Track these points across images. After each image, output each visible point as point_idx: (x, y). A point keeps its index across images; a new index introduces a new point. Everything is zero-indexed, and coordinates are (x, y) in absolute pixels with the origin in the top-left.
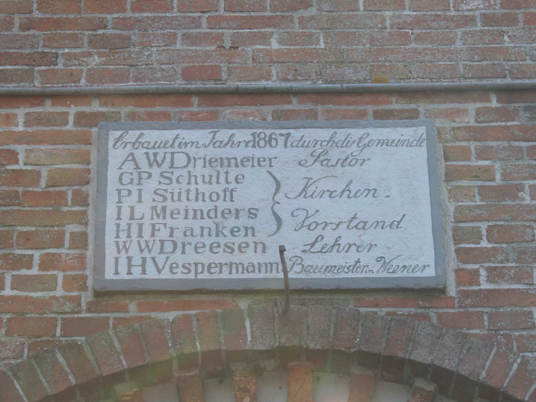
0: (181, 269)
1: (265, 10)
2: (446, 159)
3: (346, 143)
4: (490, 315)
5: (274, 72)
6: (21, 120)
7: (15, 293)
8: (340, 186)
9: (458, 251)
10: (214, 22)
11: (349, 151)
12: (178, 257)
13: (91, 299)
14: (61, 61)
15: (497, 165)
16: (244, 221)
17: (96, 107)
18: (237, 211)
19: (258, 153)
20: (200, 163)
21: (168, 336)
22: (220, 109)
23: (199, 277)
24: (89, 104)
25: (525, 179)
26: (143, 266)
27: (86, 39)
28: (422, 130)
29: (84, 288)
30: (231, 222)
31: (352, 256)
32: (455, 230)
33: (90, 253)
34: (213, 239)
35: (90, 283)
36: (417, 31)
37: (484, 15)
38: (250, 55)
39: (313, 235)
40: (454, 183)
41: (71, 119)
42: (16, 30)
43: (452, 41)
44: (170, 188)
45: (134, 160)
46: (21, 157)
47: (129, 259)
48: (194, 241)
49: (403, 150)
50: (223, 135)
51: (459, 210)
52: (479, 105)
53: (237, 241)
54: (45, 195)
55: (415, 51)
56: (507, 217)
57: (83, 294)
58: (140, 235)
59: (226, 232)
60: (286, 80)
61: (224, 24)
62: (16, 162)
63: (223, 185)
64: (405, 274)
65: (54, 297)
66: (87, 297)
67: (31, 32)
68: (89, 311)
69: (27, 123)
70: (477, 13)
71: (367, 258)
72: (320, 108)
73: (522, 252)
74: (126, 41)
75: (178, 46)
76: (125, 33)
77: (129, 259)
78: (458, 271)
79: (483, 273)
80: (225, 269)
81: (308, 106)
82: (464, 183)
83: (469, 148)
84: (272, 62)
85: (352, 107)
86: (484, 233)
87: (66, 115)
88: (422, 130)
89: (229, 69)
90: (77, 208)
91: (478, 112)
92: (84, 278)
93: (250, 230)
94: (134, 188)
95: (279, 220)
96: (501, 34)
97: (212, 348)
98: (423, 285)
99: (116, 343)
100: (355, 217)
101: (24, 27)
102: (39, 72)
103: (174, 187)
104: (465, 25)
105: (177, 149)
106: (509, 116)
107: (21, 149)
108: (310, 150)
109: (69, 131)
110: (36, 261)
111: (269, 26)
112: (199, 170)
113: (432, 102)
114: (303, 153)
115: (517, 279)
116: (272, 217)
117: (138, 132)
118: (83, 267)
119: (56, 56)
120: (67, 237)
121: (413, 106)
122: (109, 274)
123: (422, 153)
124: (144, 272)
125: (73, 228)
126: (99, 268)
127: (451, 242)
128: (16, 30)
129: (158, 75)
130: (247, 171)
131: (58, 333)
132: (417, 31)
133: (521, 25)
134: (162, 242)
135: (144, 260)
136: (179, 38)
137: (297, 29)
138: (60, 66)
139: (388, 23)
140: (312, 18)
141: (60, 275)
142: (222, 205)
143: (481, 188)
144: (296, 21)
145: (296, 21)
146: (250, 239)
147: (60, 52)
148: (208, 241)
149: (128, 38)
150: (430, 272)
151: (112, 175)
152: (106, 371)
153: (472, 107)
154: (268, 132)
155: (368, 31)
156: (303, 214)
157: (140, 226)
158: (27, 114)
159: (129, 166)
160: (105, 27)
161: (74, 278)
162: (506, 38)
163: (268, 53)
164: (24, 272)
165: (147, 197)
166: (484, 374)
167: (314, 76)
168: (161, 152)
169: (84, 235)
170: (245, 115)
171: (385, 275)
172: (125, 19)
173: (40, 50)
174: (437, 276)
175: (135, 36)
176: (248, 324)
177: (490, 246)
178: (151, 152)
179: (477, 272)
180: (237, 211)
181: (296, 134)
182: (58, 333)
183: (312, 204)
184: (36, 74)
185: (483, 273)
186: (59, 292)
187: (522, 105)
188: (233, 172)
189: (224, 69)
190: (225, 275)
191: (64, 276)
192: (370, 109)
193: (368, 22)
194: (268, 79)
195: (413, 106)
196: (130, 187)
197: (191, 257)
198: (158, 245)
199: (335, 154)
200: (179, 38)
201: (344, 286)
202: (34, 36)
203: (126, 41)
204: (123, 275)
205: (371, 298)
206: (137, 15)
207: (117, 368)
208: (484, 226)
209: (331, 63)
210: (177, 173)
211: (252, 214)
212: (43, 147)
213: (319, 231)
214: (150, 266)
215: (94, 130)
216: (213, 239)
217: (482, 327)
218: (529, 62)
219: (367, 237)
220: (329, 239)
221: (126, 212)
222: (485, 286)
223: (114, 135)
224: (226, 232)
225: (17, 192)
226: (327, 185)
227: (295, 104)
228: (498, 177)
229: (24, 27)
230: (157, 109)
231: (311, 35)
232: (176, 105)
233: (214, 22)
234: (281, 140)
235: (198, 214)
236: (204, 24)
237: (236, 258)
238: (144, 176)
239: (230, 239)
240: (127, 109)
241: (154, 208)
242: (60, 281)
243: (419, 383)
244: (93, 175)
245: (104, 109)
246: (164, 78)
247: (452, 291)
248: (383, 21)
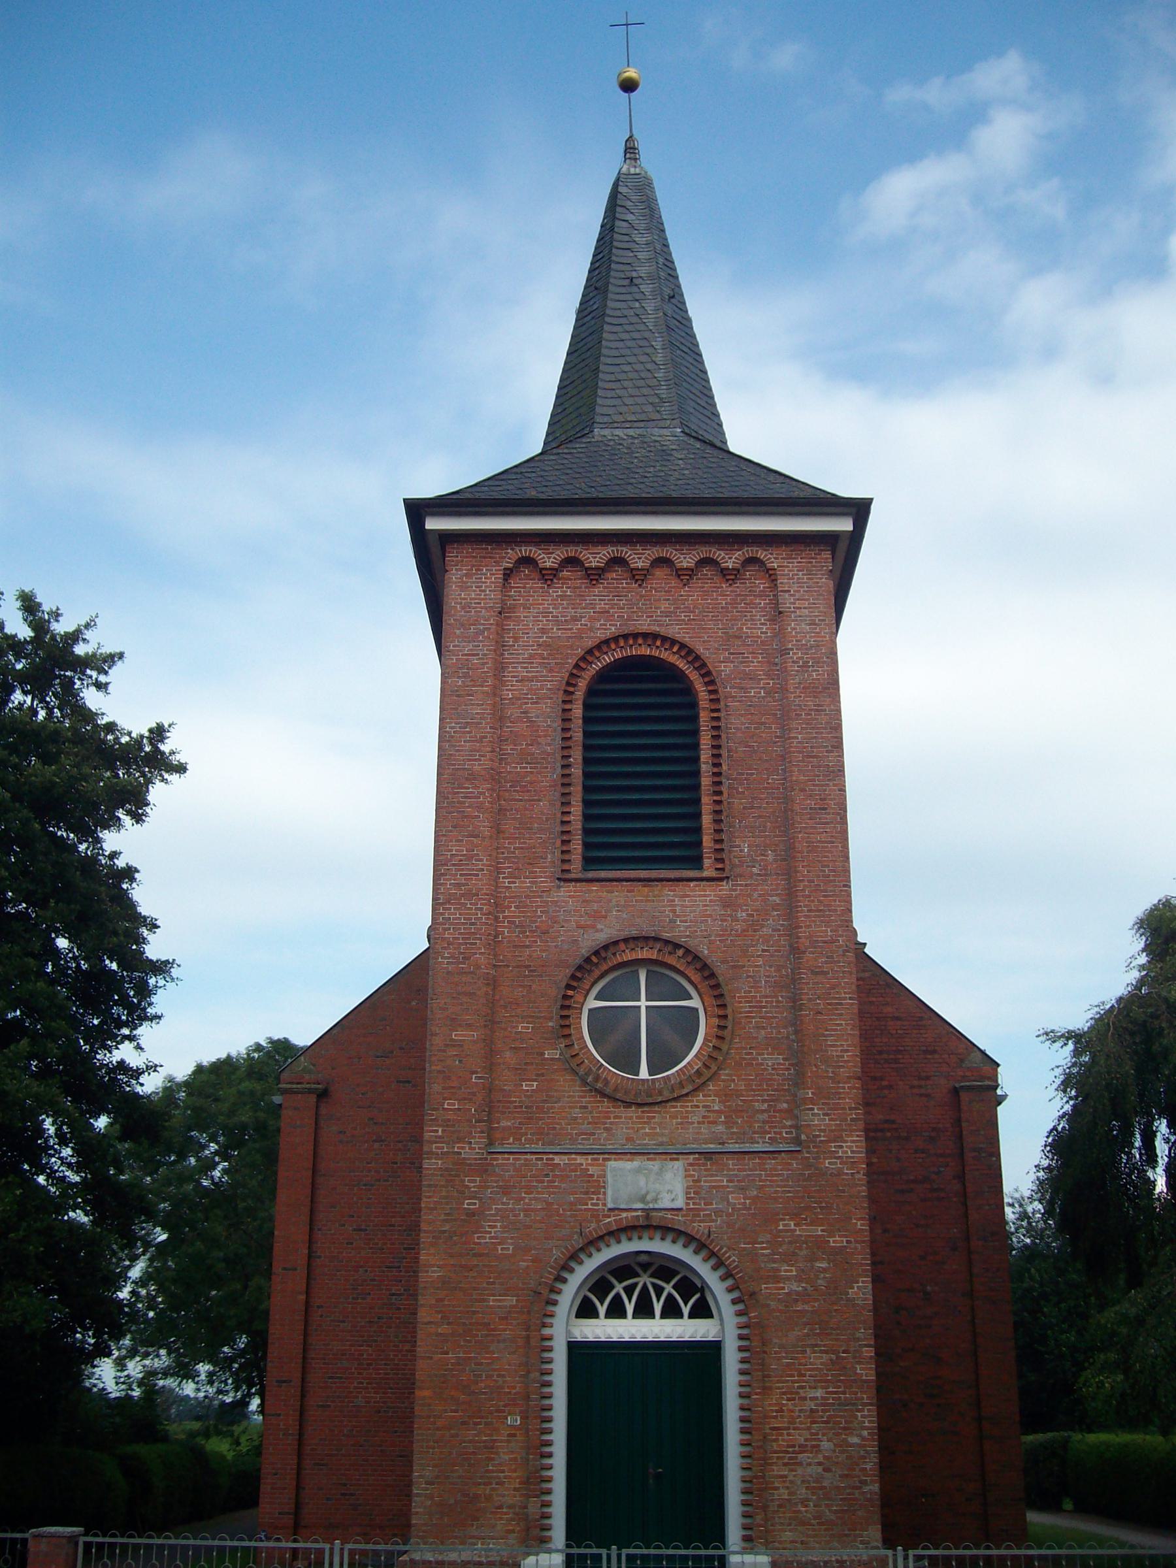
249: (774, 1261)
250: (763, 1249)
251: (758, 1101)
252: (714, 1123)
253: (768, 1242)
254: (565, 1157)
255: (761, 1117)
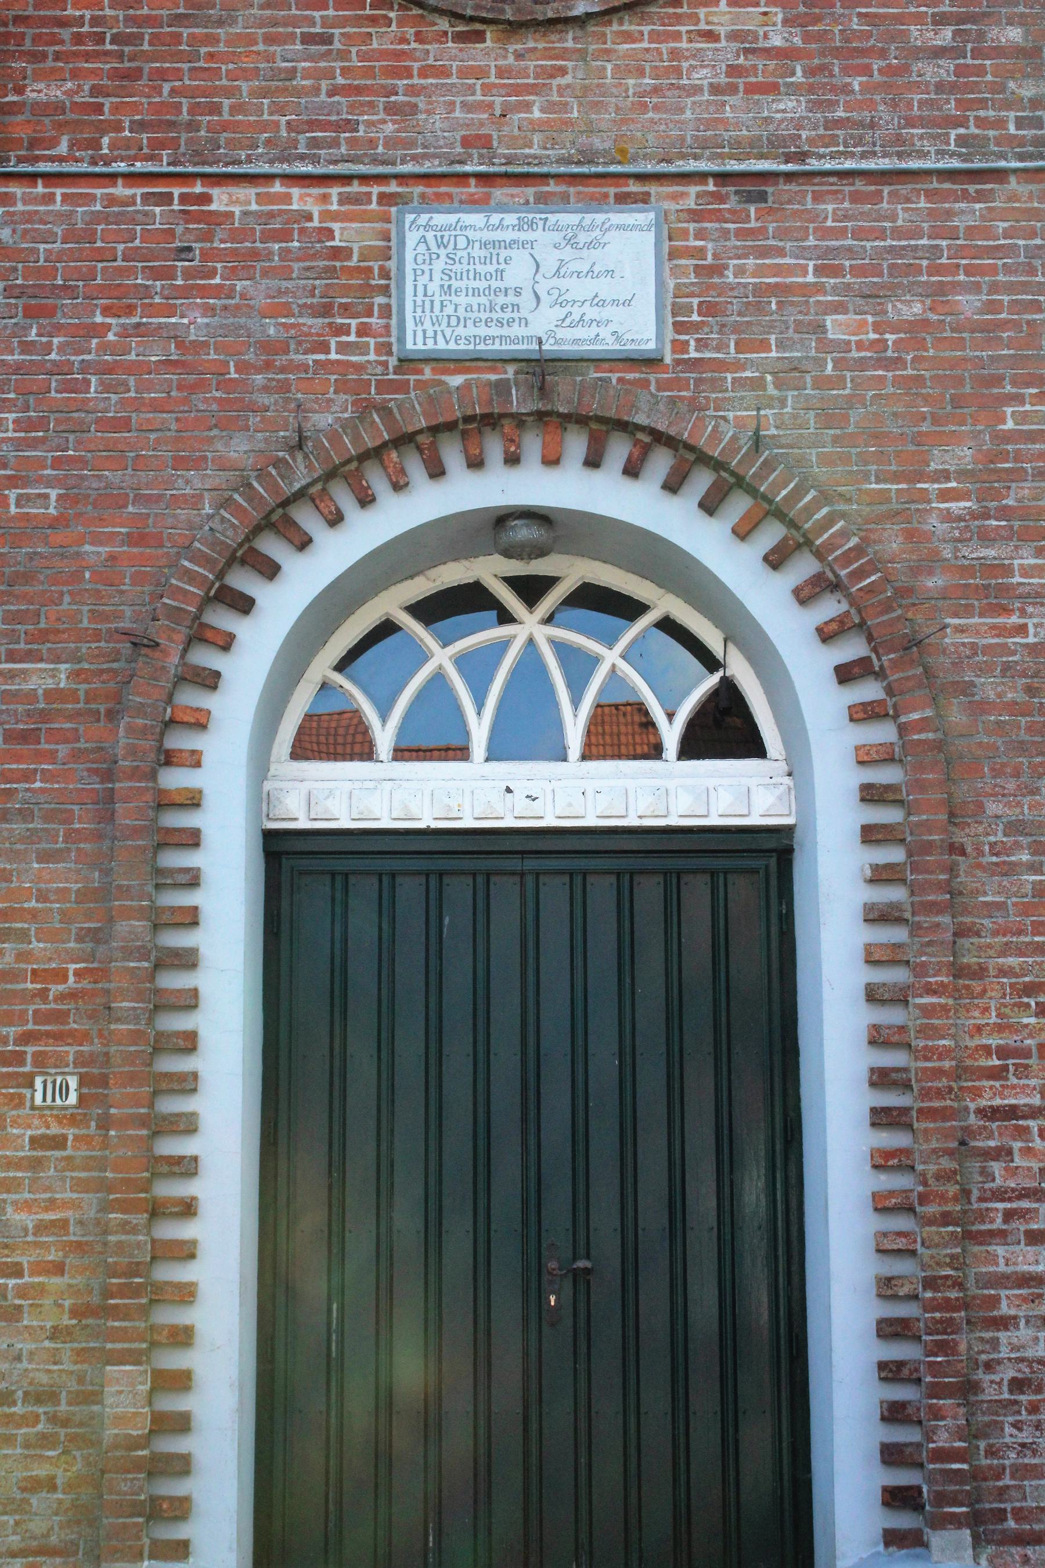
0: (463, 341)
1: (528, 77)
2: (670, 239)
3: (592, 227)
4: (695, 379)
5: (536, 141)
6: (335, 199)
7: (339, 357)
8: (585, 268)
9: (675, 324)
10: (487, 89)
11: (594, 235)
12: (460, 331)
13: (396, 363)
14: (362, 128)
15: (710, 246)
16: (511, 299)
17: (393, 187)
18: (506, 290)
19: (523, 236)
20: (477, 245)
21: (455, 400)
22: (492, 190)
23: (478, 347)
24: (388, 184)
25: (730, 258)
26: (435, 338)
27: (381, 106)
28: (652, 215)
29: (390, 353)
30: (501, 300)
31: (591, 332)
32: (674, 304)
33: (394, 322)
34: (487, 315)
35: (395, 349)
36: (654, 100)
37: (711, 85)
38: (516, 124)
39: (565, 311)
40: (675, 262)
41: (374, 198)
42: (323, 97)
43: (681, 110)
44: (454, 268)
45: (425, 242)
46: (337, 234)
47: (424, 332)
48: (473, 316)
49: (636, 234)
50: (495, 218)
51: (678, 286)
52: (699, 188)
53: (507, 316)
54: (358, 269)
55: (652, 120)
56: (714, 293)
57: (390, 359)
58: (432, 311)
59: (498, 308)
60: (546, 148)
61: (494, 91)
62: (333, 239)
63: (495, 266)
64: (633, 347)
65: (368, 362)
66: (393, 362)
67: (336, 98)
68: (395, 373)
69: (341, 202)
70: (705, 82)
71: (605, 333)
72: (572, 190)
73: (723, 326)
74: (414, 108)
75: (457, 114)
76: (413, 100)
77: (424, 332)
78: (674, 342)
79: (692, 343)
80: (497, 341)
81: (561, 188)
82: (683, 262)
83: (688, 229)
84: (534, 130)
85: (598, 190)
86: (695, 307)
87: (369, 194)
88: (652, 215)
89: (499, 137)
90: (383, 282)
91: (698, 196)
92: (390, 344)
93: (516, 307)
94: (426, 268)
95: (538, 298)
96: (724, 104)
97: (487, 411)
98: (646, 356)
99: (417, 406)
100: (596, 296)
101: (331, 94)
102: (346, 138)
103: (457, 267)
104: (694, 95)
105: (458, 232)
106: (721, 198)
107: (336, 226)
108: (563, 234)
109: (373, 211)
110: (353, 329)
111: (531, 94)
112: (477, 252)
113: (662, 185)
114: (557, 237)
115: (718, 349)
116: (533, 295)
117: (428, 216)
118: (388, 334)
119: (357, 122)
120: (376, 308)
121: (646, 189)
122: (410, 345)
123: (650, 237)
124: (436, 343)
125: (380, 300)
126: (401, 340)
127: (670, 315)
128: (323, 97)
129: (441, 143)
130: (513, 253)
131: (373, 391)
132: (654, 100)
133: (741, 94)
134: (449, 317)
135: (435, 332)
136: (458, 105)
137: (555, 98)
138: (361, 133)
139: (631, 92)
140: (568, 86)
141: (372, 341)
142: (495, 284)
143: (697, 266)
144: (555, 88)
145: (555, 88)
146: (515, 315)
147: (361, 118)
148: (484, 316)
149: (416, 105)
150: (652, 345)
151: (409, 256)
152: (410, 429)
153: (693, 190)
154: (531, 216)
155: (614, 100)
156: (556, 292)
157: (432, 302)
158: (340, 194)
159: (422, 248)
160: (397, 94)
161: (383, 344)
162: (728, 108)
163: (531, 122)
164: (344, 338)
165: (437, 276)
166: (686, 435)
167: (568, 145)
168: (446, 234)
169: (388, 306)
170: (512, 196)
171: (617, 347)
172: (412, 86)
173: (344, 117)
174: (657, 350)
175: (421, 102)
176: (514, 392)
177: (699, 319)
178: (439, 234)
179: (687, 342)
180: (506, 290)
181: (552, 218)
182: (373, 391)
183: (563, 283)
184: (343, 142)
185: (692, 343)
186: (372, 357)
187: (733, 189)
188: (504, 254)
189: (495, 137)
190: (497, 346)
191: (376, 343)
192: (612, 191)
193: (614, 90)
194: (530, 147)
195: (646, 189)
196: (422, 267)
197: (471, 331)
198: (446, 319)
199: (583, 238)
200: (458, 105)
201: (586, 357)
202: (339, 103)
203: (414, 108)
204: (420, 346)
205: (606, 365)
206: (422, 81)
207: (418, 427)
208: (695, 301)
209: (581, 132)
210: (460, 254)
211: (518, 292)
212: (354, 225)
213: (568, 309)
214: (440, 337)
215: (393, 209)
216: (487, 315)
217: (688, 389)
218: (745, 132)
219: (608, 312)
220: (576, 317)
221: (420, 290)
222: (693, 354)
223: (410, 218)
224: (498, 308)
225: (335, 267)
226: (573, 266)
227: (552, 187)
228: (710, 257)
229: (331, 94)
230: (443, 189)
231: (566, 104)
232: (457, 185)
233: (487, 89)
234: (541, 223)
235: (477, 293)
236: (479, 92)
237: (505, 331)
238: (434, 256)
239: (501, 315)
240: (418, 189)
241: (442, 286)
242: (372, 347)
243: (640, 436)
244: (394, 251)
245: (399, 190)
246: (446, 146)
247: (668, 359)
248: (627, 90)
249: (986, 537)
250: (945, 495)
251: (919, 19)
252: (770, 89)
253: (962, 474)
254: (248, 193)
255: (934, 72)
